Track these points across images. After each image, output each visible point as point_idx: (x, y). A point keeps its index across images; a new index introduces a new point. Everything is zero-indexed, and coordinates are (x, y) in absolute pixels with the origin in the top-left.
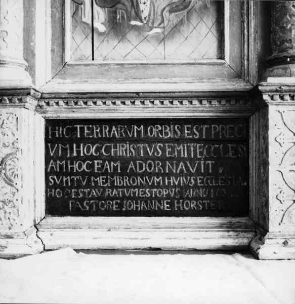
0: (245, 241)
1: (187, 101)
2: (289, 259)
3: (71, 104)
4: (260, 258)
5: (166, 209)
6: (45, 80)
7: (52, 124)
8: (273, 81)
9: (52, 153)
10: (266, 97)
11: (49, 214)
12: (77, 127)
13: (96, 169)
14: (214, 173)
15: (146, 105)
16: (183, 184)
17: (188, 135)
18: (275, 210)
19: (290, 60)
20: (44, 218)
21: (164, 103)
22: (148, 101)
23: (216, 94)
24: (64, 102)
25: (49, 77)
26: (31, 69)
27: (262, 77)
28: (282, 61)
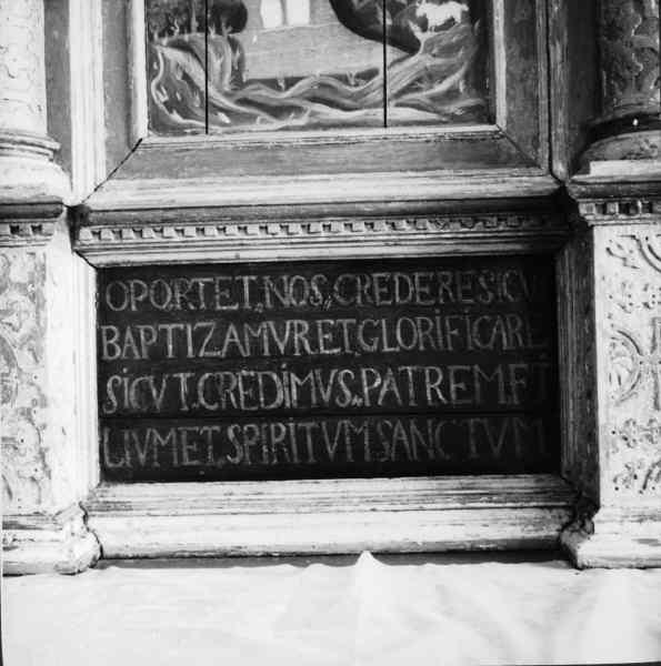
0: (551, 531)
1: (214, 227)
2: (32, 540)
3: (612, 210)
4: (579, 562)
5: (187, 462)
6: (85, 178)
7: (109, 278)
8: (601, 170)
9: (282, 340)
10: (587, 210)
11: (107, 480)
12: (242, 282)
13: (217, 381)
14: (458, 378)
15: (127, 239)
16: (433, 400)
17: (382, 299)
18: (614, 462)
19: (639, 123)
20: (40, 489)
21: (269, 229)
22: (172, 230)
23: (509, 202)
24: (113, 232)
25: (102, 176)
26: (62, 156)
27: (578, 165)
28: (622, 126)
